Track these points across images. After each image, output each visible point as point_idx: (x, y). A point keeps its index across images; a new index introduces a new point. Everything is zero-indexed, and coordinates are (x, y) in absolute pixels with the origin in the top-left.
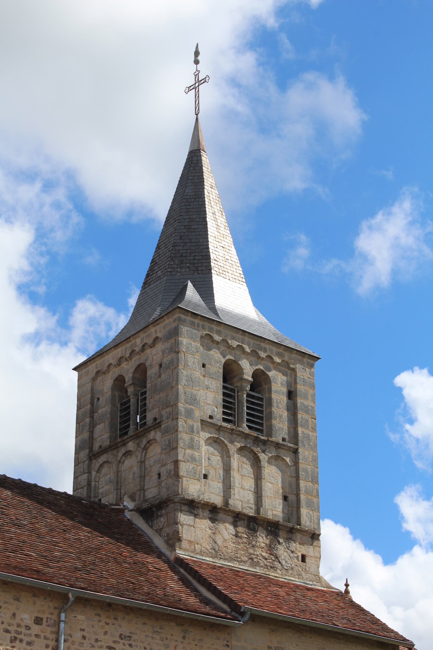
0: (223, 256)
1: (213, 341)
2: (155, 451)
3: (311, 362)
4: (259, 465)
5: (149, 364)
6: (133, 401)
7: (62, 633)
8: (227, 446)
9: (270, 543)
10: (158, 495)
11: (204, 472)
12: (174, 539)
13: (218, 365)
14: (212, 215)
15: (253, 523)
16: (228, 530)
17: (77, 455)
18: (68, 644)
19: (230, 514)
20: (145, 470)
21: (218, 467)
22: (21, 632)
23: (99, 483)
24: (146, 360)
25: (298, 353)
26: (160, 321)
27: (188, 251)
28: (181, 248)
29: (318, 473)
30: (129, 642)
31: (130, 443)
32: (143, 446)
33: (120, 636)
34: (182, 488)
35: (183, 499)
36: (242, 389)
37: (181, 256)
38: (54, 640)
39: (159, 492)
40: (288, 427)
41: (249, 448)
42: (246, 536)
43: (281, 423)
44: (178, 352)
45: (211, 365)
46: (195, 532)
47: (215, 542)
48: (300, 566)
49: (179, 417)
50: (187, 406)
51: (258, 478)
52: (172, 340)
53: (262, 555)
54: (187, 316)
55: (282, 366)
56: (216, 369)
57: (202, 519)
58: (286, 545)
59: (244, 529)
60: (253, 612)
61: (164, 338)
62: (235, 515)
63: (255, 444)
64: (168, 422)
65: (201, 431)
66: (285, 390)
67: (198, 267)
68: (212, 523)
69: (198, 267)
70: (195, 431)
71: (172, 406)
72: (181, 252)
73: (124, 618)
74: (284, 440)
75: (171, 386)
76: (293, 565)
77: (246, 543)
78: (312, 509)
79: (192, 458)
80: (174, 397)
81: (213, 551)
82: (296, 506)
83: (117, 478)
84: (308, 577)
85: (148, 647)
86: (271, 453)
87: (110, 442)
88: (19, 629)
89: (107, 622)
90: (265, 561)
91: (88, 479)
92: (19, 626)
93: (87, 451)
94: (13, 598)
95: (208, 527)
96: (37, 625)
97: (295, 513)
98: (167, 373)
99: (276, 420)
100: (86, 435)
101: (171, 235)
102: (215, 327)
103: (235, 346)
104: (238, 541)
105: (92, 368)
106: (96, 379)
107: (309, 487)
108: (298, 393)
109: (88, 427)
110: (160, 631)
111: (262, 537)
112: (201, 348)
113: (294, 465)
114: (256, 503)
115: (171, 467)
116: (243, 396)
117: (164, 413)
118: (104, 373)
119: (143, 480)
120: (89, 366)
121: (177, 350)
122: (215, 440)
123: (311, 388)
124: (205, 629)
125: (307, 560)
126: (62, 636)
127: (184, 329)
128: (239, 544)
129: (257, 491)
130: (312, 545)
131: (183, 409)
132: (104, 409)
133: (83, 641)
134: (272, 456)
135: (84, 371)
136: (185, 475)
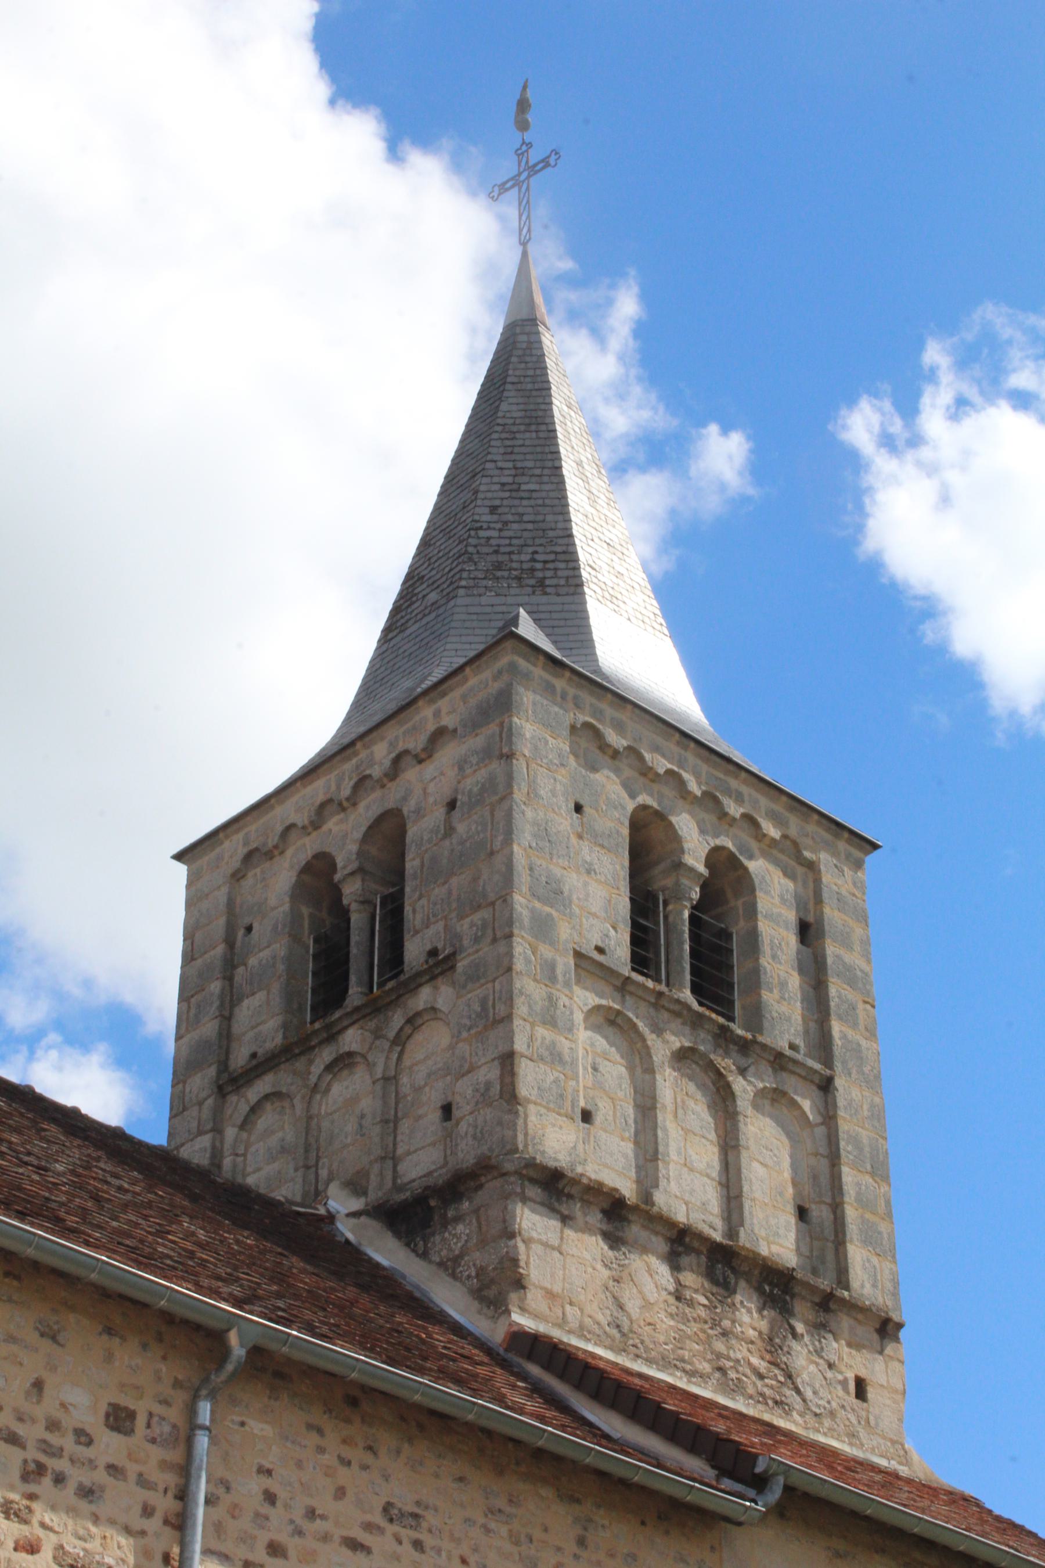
0: (609, 562)
1: (603, 746)
2: (432, 1044)
3: (857, 853)
4: (731, 1109)
5: (412, 809)
6: (357, 919)
7: (200, 1469)
8: (644, 1040)
9: (771, 1329)
10: (441, 1168)
11: (582, 1103)
12: (499, 1284)
13: (616, 813)
14: (574, 465)
15: (720, 1262)
16: (657, 1277)
17: (180, 1086)
18: (220, 1512)
19: (659, 1228)
20: (397, 1104)
21: (621, 1094)
22: (62, 1449)
23: (245, 1160)
24: (405, 799)
25: (824, 822)
26: (450, 682)
27: (515, 542)
28: (495, 534)
29: (887, 1153)
30: (415, 1535)
31: (350, 1032)
32: (392, 1035)
33: (387, 1508)
34: (526, 1134)
35: (531, 1164)
36: (678, 895)
37: (496, 552)
38: (170, 1494)
39: (445, 1157)
40: (803, 1016)
41: (704, 1056)
42: (705, 1302)
43: (785, 1003)
44: (509, 757)
45: (597, 811)
46: (564, 1269)
47: (621, 1307)
48: (853, 1410)
49: (516, 931)
50: (538, 905)
51: (729, 1145)
52: (491, 726)
53: (749, 1364)
54: (535, 665)
55: (782, 851)
56: (610, 824)
57: (583, 1231)
58: (813, 1344)
59: (700, 1279)
60: (795, 1480)
61: (465, 726)
62: (674, 1234)
63: (720, 1046)
64: (477, 951)
65: (576, 984)
66: (791, 916)
67: (545, 578)
68: (611, 1248)
69: (545, 578)
70: (560, 978)
71: (493, 904)
72: (493, 542)
73: (398, 1452)
74: (793, 1047)
75: (492, 849)
76: (834, 1404)
77: (706, 1322)
78: (878, 1250)
79: (551, 1054)
80: (496, 877)
81: (614, 1332)
82: (832, 1238)
83: (307, 1134)
84: (875, 1443)
85: (472, 1559)
86: (763, 1081)
87: (285, 1037)
88: (54, 1439)
89: (343, 1455)
90: (759, 1383)
91: (214, 1147)
92: (53, 1425)
93: (212, 1071)
94: (37, 1329)
95: (599, 1257)
96: (115, 1434)
97: (830, 1256)
98: (475, 817)
99: (771, 991)
100: (209, 1028)
101: (464, 508)
102: (609, 712)
103: (661, 771)
104: (684, 1313)
105: (234, 848)
106: (244, 876)
107: (867, 1187)
108: (827, 928)
109: (216, 1004)
110: (508, 1509)
111: (749, 1311)
112: (572, 760)
113: (822, 1124)
114: (726, 1215)
115: (489, 1073)
116: (681, 913)
117: (466, 926)
118: (269, 855)
119: (391, 1130)
120: (222, 843)
121: (505, 750)
122: (612, 1018)
123: (858, 920)
124: (643, 1523)
125: (871, 1393)
126: (199, 1477)
127: (527, 698)
128: (686, 1320)
129: (728, 1179)
130: (881, 1352)
131: (525, 912)
132: (265, 954)
133: (266, 1509)
134: (765, 1088)
135: (206, 859)
136: (533, 1098)
